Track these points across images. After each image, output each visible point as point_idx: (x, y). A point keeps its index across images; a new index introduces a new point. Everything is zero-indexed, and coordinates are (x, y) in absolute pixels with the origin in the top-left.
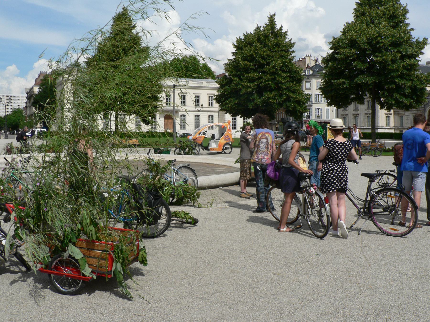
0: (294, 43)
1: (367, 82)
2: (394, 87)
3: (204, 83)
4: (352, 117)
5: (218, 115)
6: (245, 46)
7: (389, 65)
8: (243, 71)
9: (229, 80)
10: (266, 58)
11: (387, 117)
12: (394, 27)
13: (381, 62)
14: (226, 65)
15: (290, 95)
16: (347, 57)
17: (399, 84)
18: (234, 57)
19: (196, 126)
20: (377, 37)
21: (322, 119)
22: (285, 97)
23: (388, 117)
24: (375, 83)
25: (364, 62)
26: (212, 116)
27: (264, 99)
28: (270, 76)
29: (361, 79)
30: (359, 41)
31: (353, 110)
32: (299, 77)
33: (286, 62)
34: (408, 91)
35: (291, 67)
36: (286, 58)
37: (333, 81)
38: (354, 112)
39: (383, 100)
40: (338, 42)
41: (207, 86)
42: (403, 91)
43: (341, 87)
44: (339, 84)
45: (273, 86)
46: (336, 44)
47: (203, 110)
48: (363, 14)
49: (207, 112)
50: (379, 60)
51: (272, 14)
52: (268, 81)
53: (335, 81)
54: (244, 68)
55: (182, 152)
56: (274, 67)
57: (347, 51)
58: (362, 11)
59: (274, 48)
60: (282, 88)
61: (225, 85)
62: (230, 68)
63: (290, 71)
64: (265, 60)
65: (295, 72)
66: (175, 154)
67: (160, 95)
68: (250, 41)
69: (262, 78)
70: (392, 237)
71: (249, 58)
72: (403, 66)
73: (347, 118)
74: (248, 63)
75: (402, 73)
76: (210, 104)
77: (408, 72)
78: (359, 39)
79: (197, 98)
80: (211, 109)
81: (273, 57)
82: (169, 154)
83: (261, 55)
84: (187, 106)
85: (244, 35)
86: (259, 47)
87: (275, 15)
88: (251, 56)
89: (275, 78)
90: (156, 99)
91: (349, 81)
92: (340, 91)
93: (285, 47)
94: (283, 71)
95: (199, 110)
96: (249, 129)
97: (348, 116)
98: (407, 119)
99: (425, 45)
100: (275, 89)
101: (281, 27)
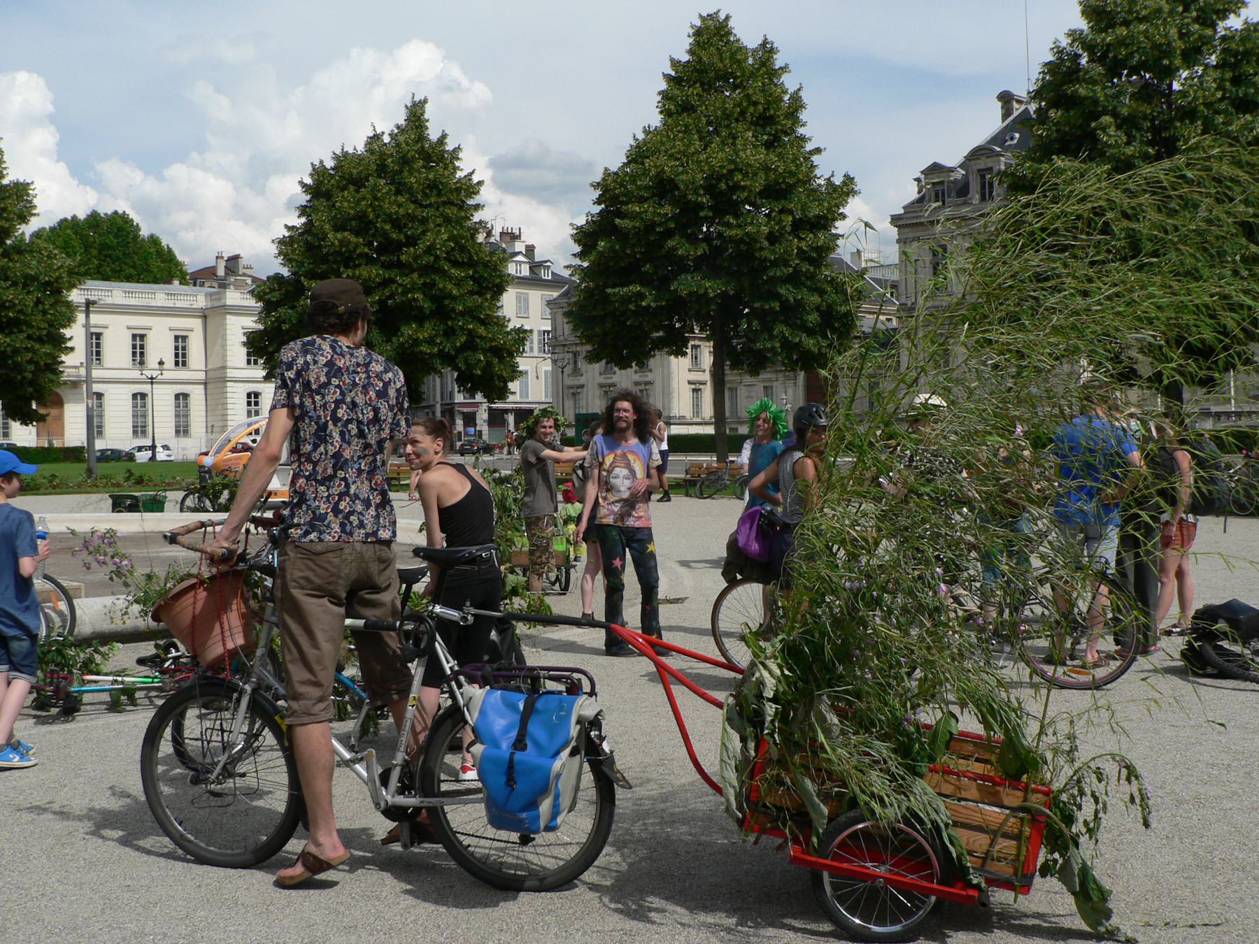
0: (480, 183)
1: (706, 293)
2: (776, 305)
3: (159, 295)
4: (598, 392)
5: (203, 391)
6: (338, 187)
7: (762, 249)
8: (335, 262)
9: (290, 288)
10: (405, 225)
11: (694, 390)
12: (769, 145)
13: (741, 241)
14: (279, 242)
15: (477, 332)
16: (650, 227)
17: (787, 300)
18: (303, 220)
19: (137, 427)
20: (731, 172)
21: (530, 400)
22: (463, 339)
23: (695, 391)
24: (724, 295)
25: (693, 239)
26: (186, 396)
27: (402, 344)
28: (420, 276)
29: (685, 285)
30: (683, 181)
31: (600, 374)
32: (498, 281)
33: (463, 237)
34: (813, 318)
35: (476, 253)
36: (462, 227)
37: (609, 291)
38: (602, 380)
39: (738, 344)
40: (623, 180)
41: (170, 304)
42: (801, 319)
43: (632, 307)
44: (627, 300)
45: (427, 305)
46: (615, 189)
47: (163, 377)
48: (687, 108)
49: (171, 383)
50: (737, 235)
51: (417, 99)
52: (412, 290)
53: (617, 290)
54: (339, 253)
55: (208, 503)
56: (430, 250)
57: (648, 210)
58: (682, 100)
59: (426, 195)
60: (453, 310)
61: (278, 304)
62: (293, 251)
63: (471, 264)
64: (400, 231)
65: (486, 265)
66: (181, 510)
67: (67, 332)
68: (355, 171)
69: (392, 281)
70: (1074, 691)
71: (354, 223)
72: (799, 249)
73: (583, 396)
74: (353, 239)
75: (797, 270)
76: (180, 359)
77: (812, 269)
78: (684, 177)
79: (138, 343)
80: (182, 374)
81: (424, 221)
82: (162, 511)
83: (390, 215)
84: (195, 368)
85: (336, 157)
86: (384, 191)
87: (425, 101)
88: (361, 217)
89: (433, 285)
90: (59, 343)
91: (654, 289)
92: (628, 319)
93: (455, 194)
94: (455, 264)
95: (152, 378)
96: (550, 427)
97: (585, 390)
98: (748, 397)
99: (847, 195)
100: (434, 314)
101: (444, 136)
